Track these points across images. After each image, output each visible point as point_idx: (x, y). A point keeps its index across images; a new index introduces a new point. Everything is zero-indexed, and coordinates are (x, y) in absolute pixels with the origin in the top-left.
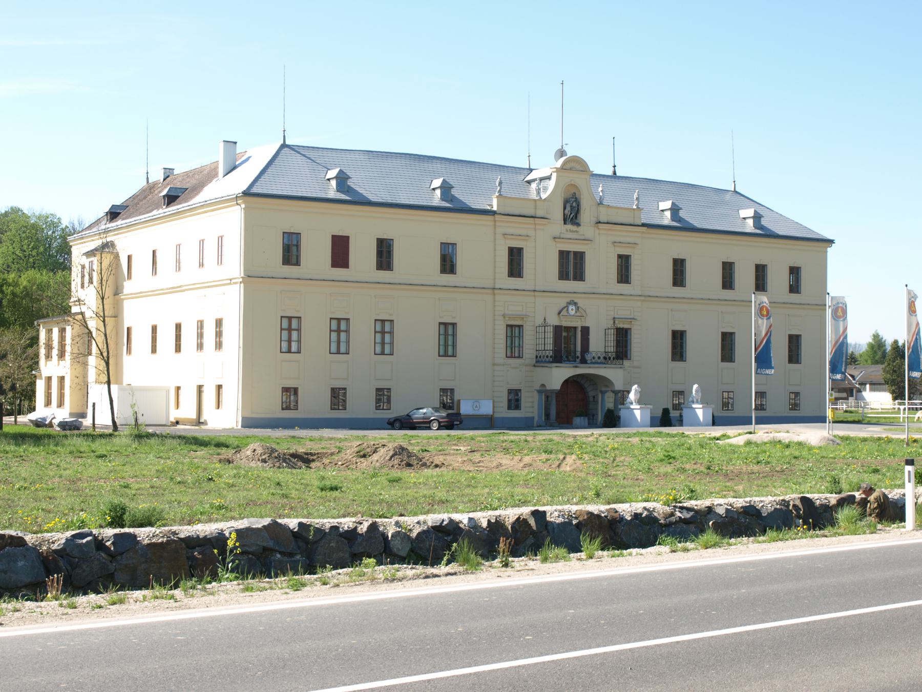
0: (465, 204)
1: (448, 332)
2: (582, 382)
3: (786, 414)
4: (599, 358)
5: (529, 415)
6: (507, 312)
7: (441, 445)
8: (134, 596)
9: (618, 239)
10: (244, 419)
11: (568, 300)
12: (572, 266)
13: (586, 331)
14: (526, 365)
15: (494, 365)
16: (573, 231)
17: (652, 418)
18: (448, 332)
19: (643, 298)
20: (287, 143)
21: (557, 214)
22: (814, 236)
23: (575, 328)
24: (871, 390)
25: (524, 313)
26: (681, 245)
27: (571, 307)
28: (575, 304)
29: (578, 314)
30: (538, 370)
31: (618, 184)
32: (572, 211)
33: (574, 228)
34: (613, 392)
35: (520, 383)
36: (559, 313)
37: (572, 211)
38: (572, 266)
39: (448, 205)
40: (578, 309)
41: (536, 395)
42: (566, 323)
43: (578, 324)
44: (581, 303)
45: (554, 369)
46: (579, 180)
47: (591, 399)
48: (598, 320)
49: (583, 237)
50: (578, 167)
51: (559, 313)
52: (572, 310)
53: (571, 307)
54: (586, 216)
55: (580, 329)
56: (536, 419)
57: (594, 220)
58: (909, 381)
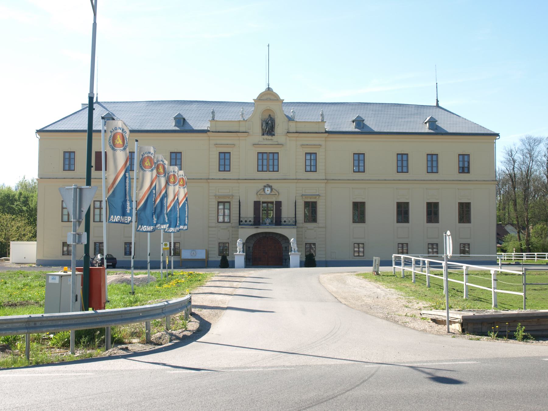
0: (443, 130)
1: (359, 211)
3: (351, 259)
4: (250, 221)
6: (217, 194)
7: (11, 274)
9: (218, 142)
10: (37, 260)
11: (265, 184)
12: (268, 161)
15: (209, 227)
16: (268, 139)
17: (301, 262)
18: (359, 211)
19: (296, 181)
20: (99, 101)
21: (257, 128)
22: (486, 132)
25: (231, 194)
26: (361, 144)
27: (266, 189)
29: (273, 193)
31: (438, 109)
32: (269, 127)
33: (270, 137)
35: (228, 239)
37: (269, 127)
38: (268, 161)
39: (432, 131)
40: (272, 190)
42: (262, 200)
43: (274, 199)
44: (274, 186)
46: (272, 106)
47: (284, 249)
48: (290, 197)
49: (276, 143)
50: (272, 98)
52: (268, 190)
54: (279, 129)
57: (287, 131)
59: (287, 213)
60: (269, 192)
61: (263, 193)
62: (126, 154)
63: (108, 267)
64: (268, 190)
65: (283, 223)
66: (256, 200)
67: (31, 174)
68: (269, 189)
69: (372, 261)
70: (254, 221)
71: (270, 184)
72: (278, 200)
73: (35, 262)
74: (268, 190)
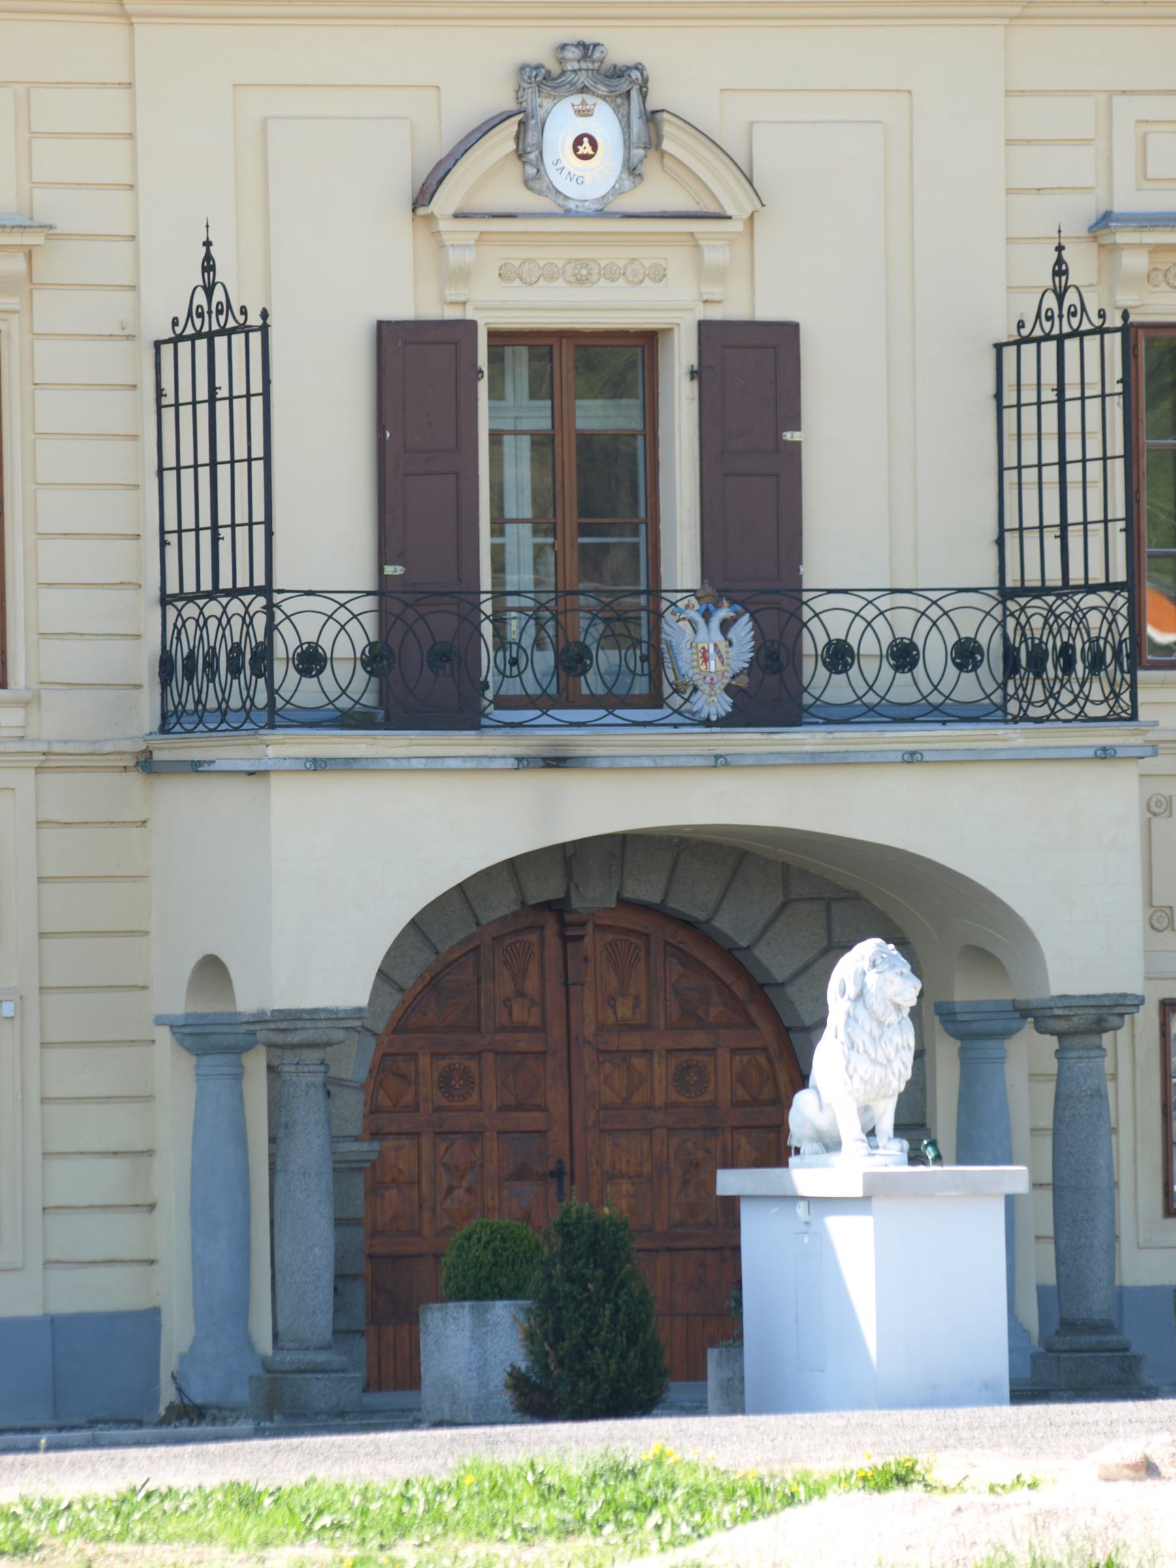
2: (732, 924)
5: (111, 1293)
8: (549, 1433)
11: (535, 44)
13: (755, 368)
14: (47, 762)
23: (648, 342)
24: (797, 427)
27: (562, 121)
28: (622, 83)
30: (177, 796)
34: (1038, 1015)
36: (423, 196)
40: (648, 130)
41: (171, 1073)
42: (508, 293)
43: (667, 295)
45: (290, 797)
51: (423, 196)
52: (583, 153)
53: (562, 121)
55: (683, 353)
56: (178, 1335)
58: (607, 545)
59: (897, 506)
60: (593, 179)
61: (509, 192)
62: (10, 1505)
63: (634, 435)
64: (585, 146)
65: (817, 679)
66: (403, 309)
67: (709, 1350)
68: (604, 123)
69: (1010, 1162)
70: (375, 660)
71: (621, 46)
72: (735, 310)
73: (617, 652)
74: (585, 146)
